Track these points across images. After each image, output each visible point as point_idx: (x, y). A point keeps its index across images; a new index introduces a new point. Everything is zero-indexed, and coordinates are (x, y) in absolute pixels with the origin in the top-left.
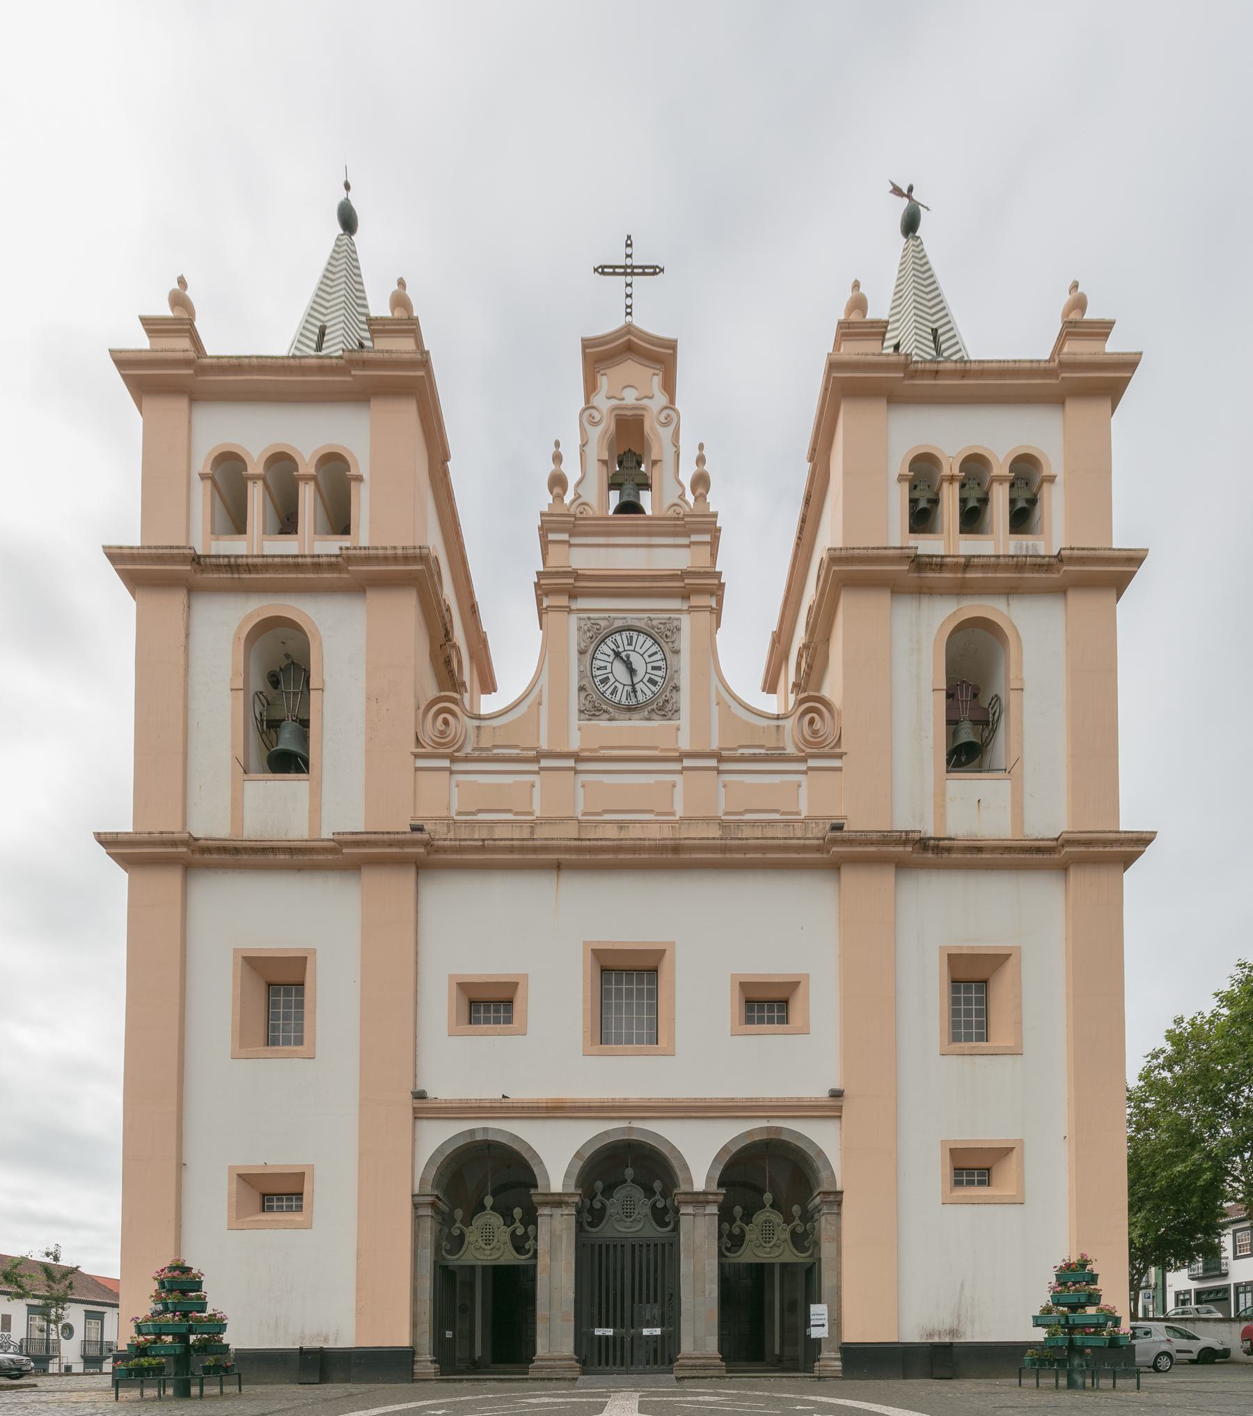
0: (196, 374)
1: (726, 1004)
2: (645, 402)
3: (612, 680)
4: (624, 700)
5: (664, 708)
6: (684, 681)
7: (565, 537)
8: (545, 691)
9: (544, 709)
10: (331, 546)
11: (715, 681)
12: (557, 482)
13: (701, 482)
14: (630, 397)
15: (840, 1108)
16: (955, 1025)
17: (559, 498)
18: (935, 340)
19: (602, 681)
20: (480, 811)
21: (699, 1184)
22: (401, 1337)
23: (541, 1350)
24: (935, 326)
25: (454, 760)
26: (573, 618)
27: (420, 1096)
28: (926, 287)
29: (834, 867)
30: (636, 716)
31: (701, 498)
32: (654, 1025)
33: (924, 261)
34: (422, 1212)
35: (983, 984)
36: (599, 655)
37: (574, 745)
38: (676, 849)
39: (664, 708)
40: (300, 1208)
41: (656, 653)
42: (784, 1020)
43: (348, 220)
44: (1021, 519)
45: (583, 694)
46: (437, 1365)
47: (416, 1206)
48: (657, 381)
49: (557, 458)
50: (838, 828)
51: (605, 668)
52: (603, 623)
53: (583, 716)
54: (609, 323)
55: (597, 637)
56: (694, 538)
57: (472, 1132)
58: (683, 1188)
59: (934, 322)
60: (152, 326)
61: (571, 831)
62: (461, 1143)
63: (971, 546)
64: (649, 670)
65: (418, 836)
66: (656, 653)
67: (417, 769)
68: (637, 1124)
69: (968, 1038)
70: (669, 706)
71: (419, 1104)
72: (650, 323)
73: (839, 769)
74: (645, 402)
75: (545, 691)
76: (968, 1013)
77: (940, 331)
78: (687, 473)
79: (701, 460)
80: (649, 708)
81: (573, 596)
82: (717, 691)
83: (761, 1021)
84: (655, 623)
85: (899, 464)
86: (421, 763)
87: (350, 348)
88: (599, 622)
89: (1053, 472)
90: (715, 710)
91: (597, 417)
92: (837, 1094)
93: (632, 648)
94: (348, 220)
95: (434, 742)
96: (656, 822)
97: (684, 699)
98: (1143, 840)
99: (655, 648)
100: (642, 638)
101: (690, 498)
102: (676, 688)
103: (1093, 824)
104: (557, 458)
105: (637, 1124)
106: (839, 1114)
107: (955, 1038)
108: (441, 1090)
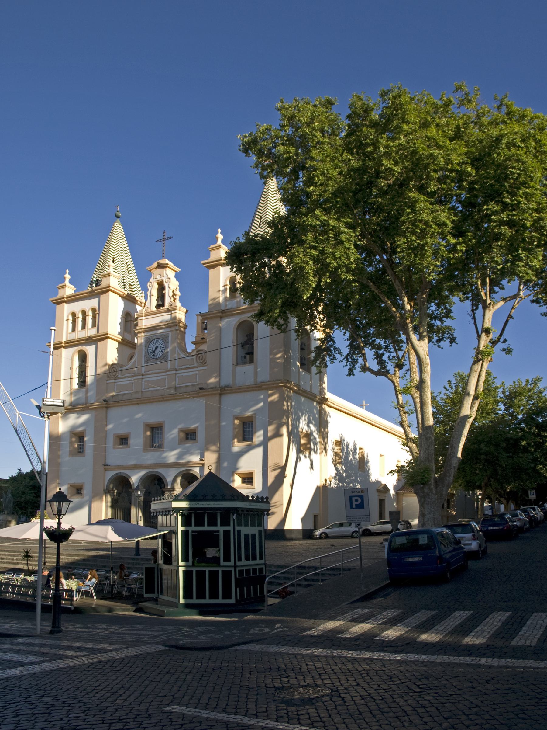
27: (105, 465)
57: (117, 473)
58: (166, 487)
71: (105, 467)
105: (155, 470)
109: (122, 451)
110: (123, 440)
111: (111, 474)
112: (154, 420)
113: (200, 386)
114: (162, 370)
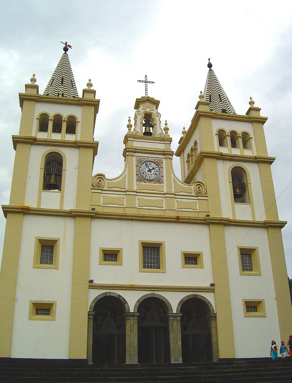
0: (39, 98)
1: (179, 260)
2: (152, 111)
3: (145, 173)
4: (148, 178)
5: (159, 181)
7: (132, 139)
8: (127, 175)
9: (127, 179)
11: (172, 175)
12: (129, 126)
13: (166, 129)
14: (148, 110)
16: (243, 266)
17: (130, 130)
18: (220, 97)
19: (142, 173)
20: (109, 204)
21: (175, 311)
24: (219, 93)
25: (102, 190)
26: (134, 157)
28: (220, 106)
30: (152, 182)
31: (166, 133)
32: (158, 262)
33: (214, 75)
34: (128, 309)
35: (250, 255)
36: (141, 167)
37: (135, 189)
39: (159, 181)
41: (157, 167)
42: (196, 263)
43: (210, 66)
44: (245, 146)
45: (137, 176)
47: (89, 315)
48: (155, 107)
49: (129, 121)
50: (93, 209)
51: (143, 170)
52: (143, 160)
53: (137, 181)
54: (141, 94)
55: (140, 162)
56: (166, 142)
57: (106, 293)
59: (219, 92)
60: (27, 86)
62: (103, 296)
64: (155, 171)
65: (93, 211)
66: (157, 167)
67: (92, 192)
68: (155, 292)
69: (247, 270)
70: (161, 181)
72: (151, 95)
74: (152, 111)
75: (127, 175)
76: (246, 263)
77: (221, 95)
78: (163, 126)
79: (166, 124)
80: (156, 181)
81: (135, 152)
82: (126, 174)
83: (189, 264)
84: (156, 160)
85: (215, 132)
86: (93, 191)
87: (64, 81)
88: (142, 159)
89: (252, 137)
90: (173, 182)
91: (140, 114)
92: (212, 285)
93: (155, 171)
94: (210, 66)
95: (97, 186)
96: (159, 210)
97: (165, 179)
98: (285, 223)
99: (157, 166)
100: (153, 164)
101: (164, 132)
102: (162, 176)
103: (271, 219)
104: (129, 121)
105: (155, 292)
106: (214, 291)
107: (243, 270)
111: (95, 294)
113: (94, 207)
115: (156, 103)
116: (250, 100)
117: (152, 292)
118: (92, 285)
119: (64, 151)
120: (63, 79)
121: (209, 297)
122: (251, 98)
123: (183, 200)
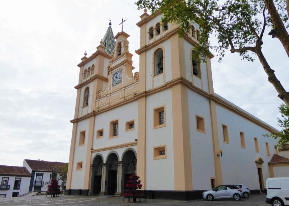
6: (123, 77)
10: (167, 32)
15: (137, 143)
22: (87, 189)
23: (101, 191)
29: (137, 99)
38: (118, 104)
40: (164, 154)
43: (110, 24)
46: (61, 176)
50: (135, 94)
61: (108, 105)
63: (167, 32)
68: (114, 150)
71: (92, 150)
73: (138, 83)
81: (112, 70)
85: (148, 31)
94: (110, 24)
105: (114, 150)
108: (95, 148)
109: (101, 139)
110: (101, 133)
111: (94, 155)
112: (114, 119)
114: (119, 89)
115: (127, 36)
116: (85, 52)
117: (112, 150)
118: (92, 151)
119: (162, 46)
120: (106, 42)
121: (135, 148)
122: (86, 52)
123: (101, 100)
